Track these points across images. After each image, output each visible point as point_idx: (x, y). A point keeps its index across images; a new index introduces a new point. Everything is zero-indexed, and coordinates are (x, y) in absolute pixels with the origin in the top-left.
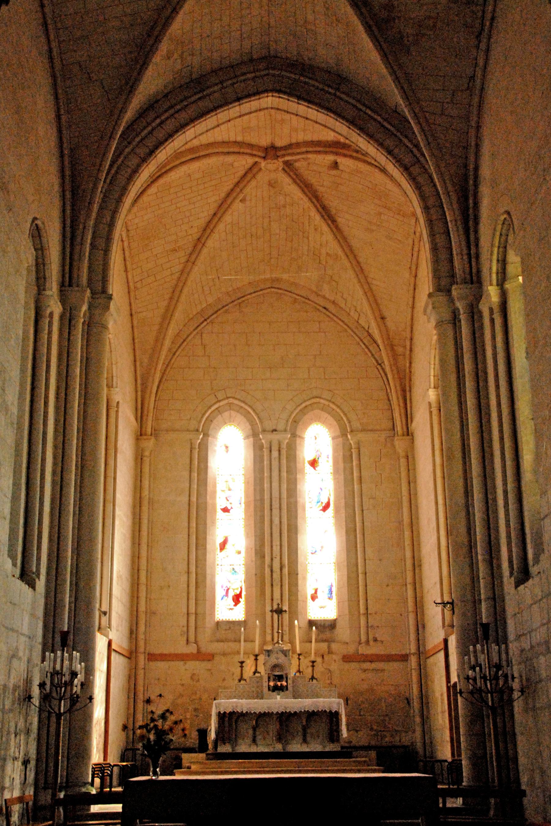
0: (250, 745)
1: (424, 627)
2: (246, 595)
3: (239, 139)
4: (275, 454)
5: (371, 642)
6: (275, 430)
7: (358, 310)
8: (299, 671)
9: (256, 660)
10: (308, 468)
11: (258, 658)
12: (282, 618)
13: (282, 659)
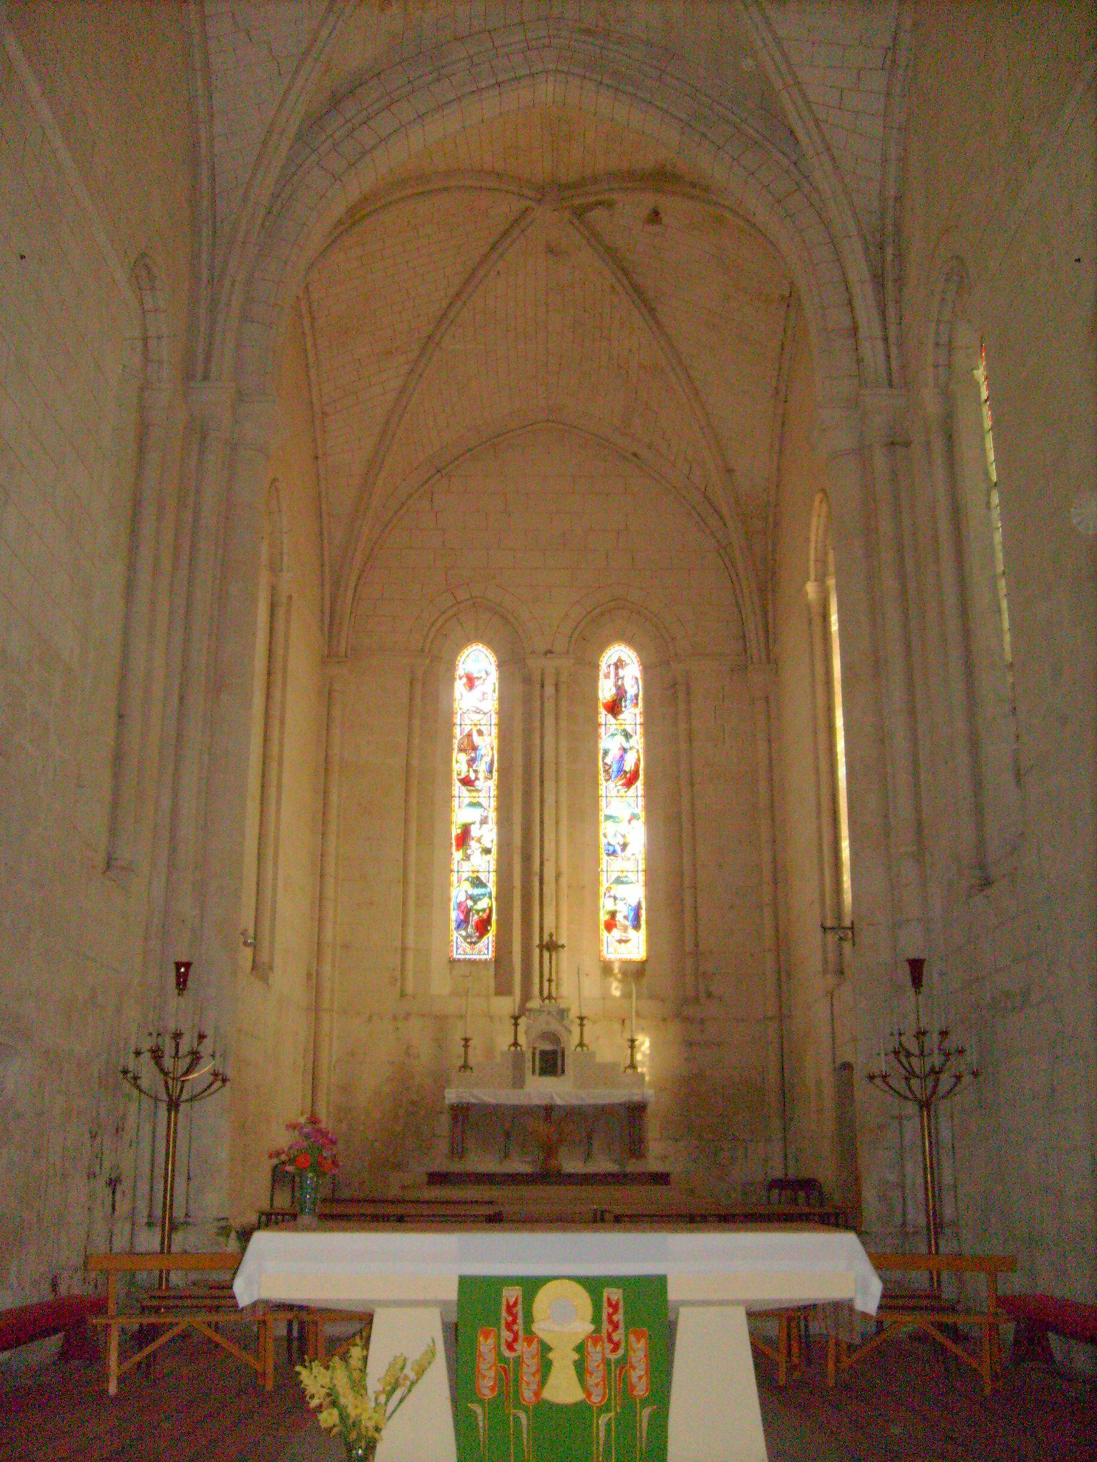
0: (501, 1163)
1: (789, 976)
2: (498, 921)
3: (499, 166)
4: (549, 690)
5: (703, 1000)
6: (551, 652)
7: (689, 458)
8: (581, 1044)
9: (516, 1025)
10: (603, 716)
11: (520, 1021)
12: (557, 959)
13: (554, 1026)
